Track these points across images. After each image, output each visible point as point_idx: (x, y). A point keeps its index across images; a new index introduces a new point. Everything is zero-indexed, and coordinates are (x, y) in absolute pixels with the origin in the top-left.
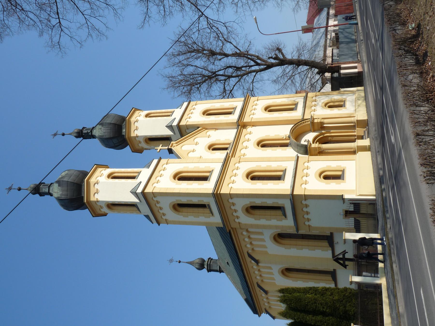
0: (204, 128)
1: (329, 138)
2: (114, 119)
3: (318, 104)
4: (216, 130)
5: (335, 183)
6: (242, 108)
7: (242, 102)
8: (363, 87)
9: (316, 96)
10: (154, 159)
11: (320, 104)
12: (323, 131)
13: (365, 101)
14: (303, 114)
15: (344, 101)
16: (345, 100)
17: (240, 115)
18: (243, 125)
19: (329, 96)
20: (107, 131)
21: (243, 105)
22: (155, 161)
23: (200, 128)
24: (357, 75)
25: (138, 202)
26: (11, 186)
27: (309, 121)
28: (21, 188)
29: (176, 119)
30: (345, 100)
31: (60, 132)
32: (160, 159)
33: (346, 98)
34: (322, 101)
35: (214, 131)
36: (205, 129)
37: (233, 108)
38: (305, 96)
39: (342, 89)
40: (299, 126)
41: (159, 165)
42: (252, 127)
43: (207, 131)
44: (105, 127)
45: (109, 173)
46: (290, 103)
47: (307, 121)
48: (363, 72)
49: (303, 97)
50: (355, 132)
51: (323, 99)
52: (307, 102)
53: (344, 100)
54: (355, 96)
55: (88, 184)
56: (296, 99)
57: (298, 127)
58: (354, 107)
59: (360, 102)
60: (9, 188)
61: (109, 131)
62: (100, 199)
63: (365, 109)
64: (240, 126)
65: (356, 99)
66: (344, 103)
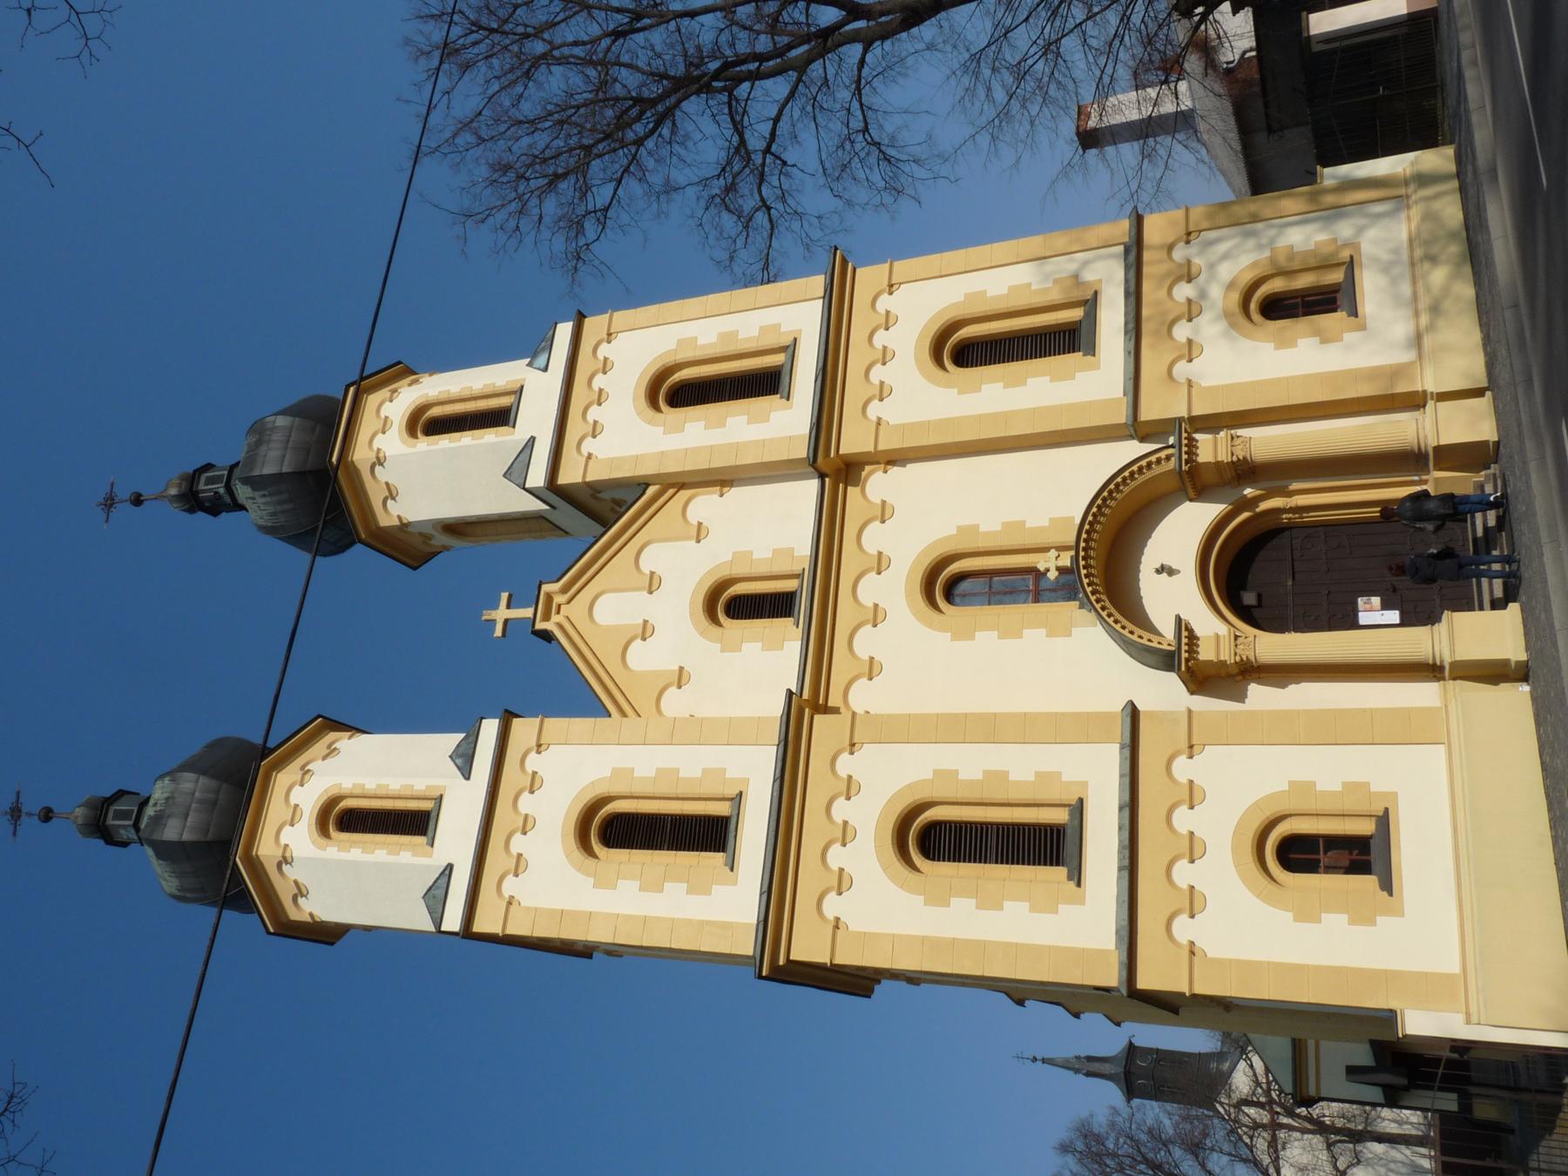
0: (671, 486)
1: (1284, 516)
2: (290, 445)
3: (1203, 294)
4: (726, 489)
5: (1344, 917)
6: (821, 365)
7: (817, 301)
8: (1449, 151)
9: (1189, 234)
10: (556, 324)
11: (1216, 292)
12: (1248, 492)
13: (1468, 270)
14: (1131, 383)
15: (1344, 263)
16: (1352, 257)
17: (814, 420)
18: (843, 466)
19: (1260, 226)
20: (279, 508)
21: (823, 347)
22: (564, 331)
23: (651, 490)
24: (1404, 30)
25: (547, 510)
26: (13, 798)
27: (1168, 458)
28: (141, 496)
29: (536, 443)
30: (1352, 257)
31: (123, 493)
32: (580, 318)
33: (1356, 246)
34: (1226, 271)
35: (716, 497)
36: (676, 490)
37: (784, 349)
38: (1127, 239)
39: (1327, 171)
40: (1119, 496)
41: (573, 400)
42: (885, 472)
43: (684, 494)
44: (266, 493)
45: (408, 414)
46: (1056, 296)
47: (1159, 461)
48: (1444, 18)
49: (1121, 248)
50: (1425, 482)
51: (1226, 256)
52: (1147, 287)
53: (1345, 255)
54: (1409, 218)
55: (353, 473)
56: (1086, 263)
57: (1115, 499)
58: (1409, 312)
59: (1438, 276)
60: (106, 500)
61: (289, 506)
62: (412, 515)
63: (1476, 336)
64: (827, 480)
65: (1418, 253)
66: (1346, 273)
